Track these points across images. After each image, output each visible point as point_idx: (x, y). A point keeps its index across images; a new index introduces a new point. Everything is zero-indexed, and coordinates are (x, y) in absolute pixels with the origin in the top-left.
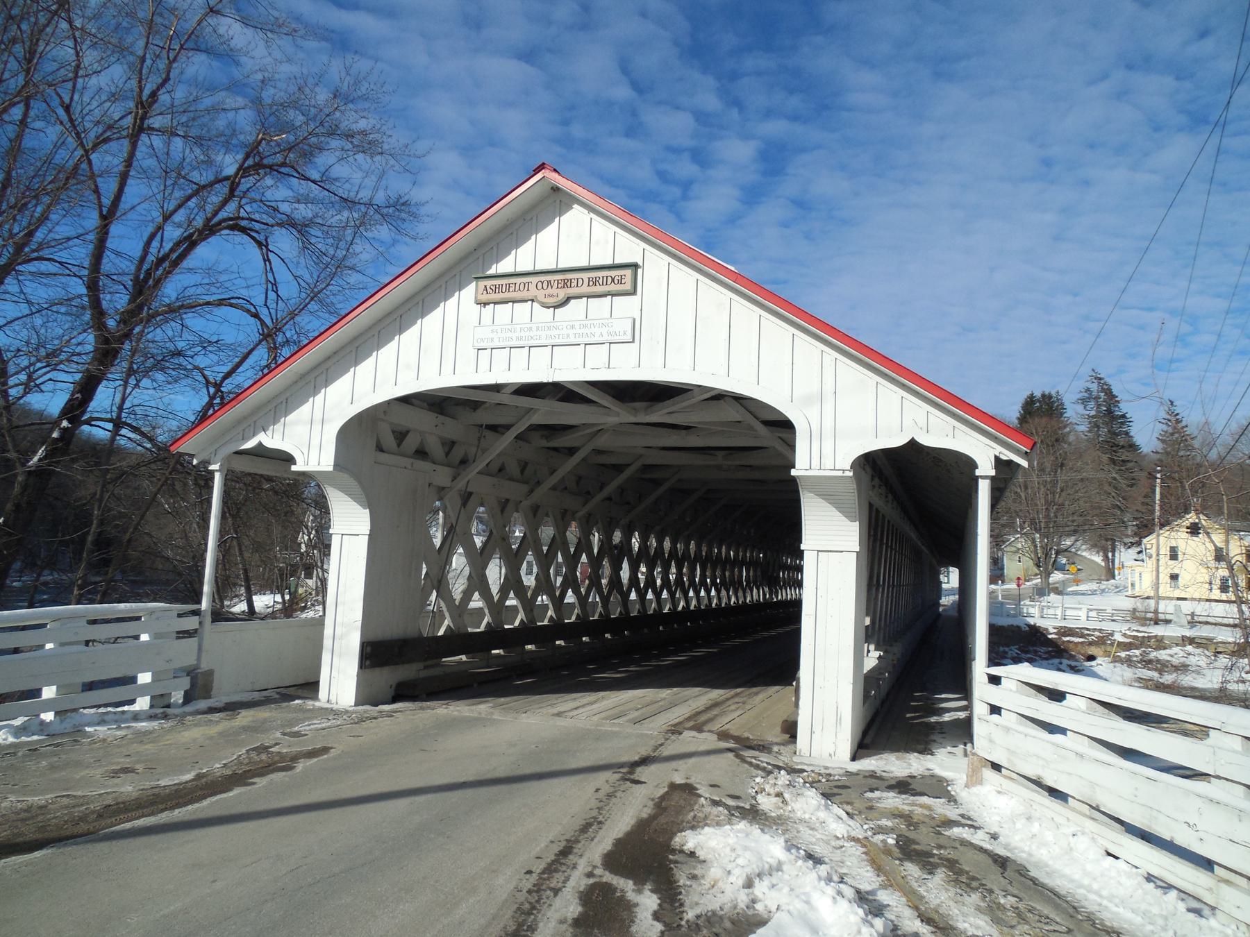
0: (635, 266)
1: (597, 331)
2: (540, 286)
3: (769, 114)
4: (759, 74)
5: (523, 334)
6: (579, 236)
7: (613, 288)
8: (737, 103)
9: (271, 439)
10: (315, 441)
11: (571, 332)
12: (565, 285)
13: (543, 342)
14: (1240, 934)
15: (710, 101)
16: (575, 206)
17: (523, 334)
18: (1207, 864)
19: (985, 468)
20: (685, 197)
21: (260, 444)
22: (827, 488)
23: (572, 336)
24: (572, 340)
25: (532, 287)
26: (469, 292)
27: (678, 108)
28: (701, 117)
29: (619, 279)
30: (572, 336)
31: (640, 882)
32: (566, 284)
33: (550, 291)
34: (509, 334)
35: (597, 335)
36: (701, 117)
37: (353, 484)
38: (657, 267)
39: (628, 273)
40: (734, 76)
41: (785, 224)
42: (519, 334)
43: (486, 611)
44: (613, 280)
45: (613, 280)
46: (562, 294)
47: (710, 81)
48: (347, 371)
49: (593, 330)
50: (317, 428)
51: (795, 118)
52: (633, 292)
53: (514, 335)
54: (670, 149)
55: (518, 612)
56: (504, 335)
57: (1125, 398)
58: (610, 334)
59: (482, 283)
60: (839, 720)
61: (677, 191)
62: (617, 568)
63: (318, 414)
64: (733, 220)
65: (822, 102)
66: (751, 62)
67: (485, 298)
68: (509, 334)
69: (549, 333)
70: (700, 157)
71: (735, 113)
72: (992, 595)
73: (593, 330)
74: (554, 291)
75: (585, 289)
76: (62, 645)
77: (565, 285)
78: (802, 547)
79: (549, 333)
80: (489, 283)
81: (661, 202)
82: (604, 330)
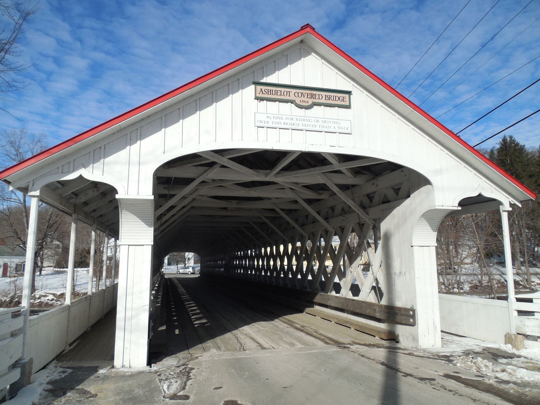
0: (349, 93)
2: (296, 94)
3: (95, 49)
4: (92, 29)
5: (288, 121)
6: (310, 70)
8: (80, 40)
9: (93, 173)
10: (134, 177)
11: (317, 124)
12: (312, 97)
13: (300, 127)
15: (66, 36)
16: (313, 54)
20: (48, 80)
21: (81, 177)
23: (318, 127)
24: (318, 129)
26: (250, 91)
27: (48, 35)
28: (60, 42)
29: (338, 99)
30: (318, 127)
32: (312, 96)
33: (302, 98)
34: (279, 121)
35: (332, 127)
36: (60, 42)
38: (360, 98)
39: (347, 96)
40: (80, 27)
41: (100, 102)
43: (356, 298)
44: (339, 99)
45: (339, 99)
46: (310, 101)
47: (66, 26)
48: (160, 130)
49: (329, 125)
50: (134, 169)
51: (108, 53)
52: (348, 107)
53: (282, 121)
54: (42, 54)
55: (336, 293)
59: (259, 87)
61: (43, 76)
63: (135, 158)
64: (73, 95)
65: (121, 50)
66: (88, 22)
67: (261, 95)
68: (279, 121)
69: (291, 121)
70: (57, 61)
71: (78, 44)
73: (329, 125)
74: (305, 99)
75: (323, 101)
77: (312, 97)
79: (291, 121)
80: (264, 88)
81: (35, 80)
82: (336, 126)
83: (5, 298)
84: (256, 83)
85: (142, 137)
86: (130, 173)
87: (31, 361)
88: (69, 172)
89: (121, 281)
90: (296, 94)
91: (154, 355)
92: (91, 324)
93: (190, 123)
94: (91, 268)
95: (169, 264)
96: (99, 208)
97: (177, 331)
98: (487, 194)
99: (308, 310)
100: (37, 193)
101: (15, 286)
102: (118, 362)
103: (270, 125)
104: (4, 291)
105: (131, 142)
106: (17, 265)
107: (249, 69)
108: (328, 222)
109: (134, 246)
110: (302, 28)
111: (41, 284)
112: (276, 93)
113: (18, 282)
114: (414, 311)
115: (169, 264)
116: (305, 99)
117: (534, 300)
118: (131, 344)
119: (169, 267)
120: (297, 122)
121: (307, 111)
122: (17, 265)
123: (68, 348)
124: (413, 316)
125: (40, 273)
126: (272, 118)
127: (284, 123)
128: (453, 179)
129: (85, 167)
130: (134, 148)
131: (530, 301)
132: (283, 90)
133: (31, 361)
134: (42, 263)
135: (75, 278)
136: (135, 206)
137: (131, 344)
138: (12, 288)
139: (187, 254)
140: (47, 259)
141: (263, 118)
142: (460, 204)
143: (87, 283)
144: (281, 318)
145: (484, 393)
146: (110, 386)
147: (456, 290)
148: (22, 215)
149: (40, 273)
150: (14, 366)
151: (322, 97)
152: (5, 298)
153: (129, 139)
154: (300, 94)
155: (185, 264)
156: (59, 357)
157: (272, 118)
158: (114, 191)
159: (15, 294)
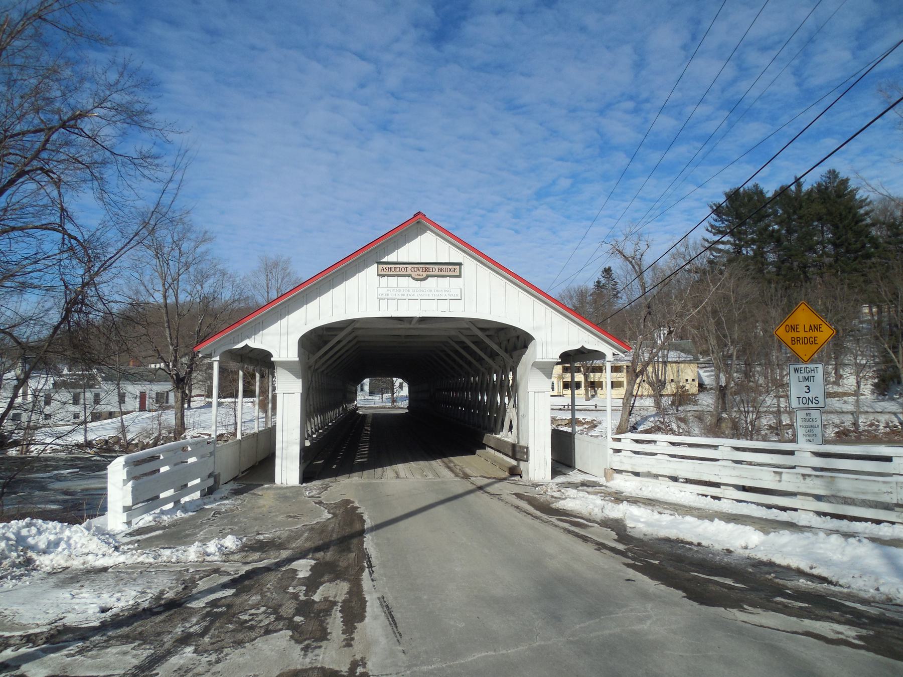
0: (460, 264)
1: (444, 294)
6: (426, 247)
7: (450, 273)
9: (254, 343)
10: (284, 344)
12: (425, 270)
13: (416, 297)
14: (901, 401)
18: (717, 485)
24: (431, 297)
29: (452, 270)
32: (427, 270)
39: (458, 267)
52: (459, 276)
59: (381, 266)
60: (546, 463)
63: (284, 331)
67: (383, 273)
72: (268, 404)
74: (421, 273)
75: (436, 273)
76: (175, 465)
77: (425, 270)
80: (384, 266)
83: (148, 440)
84: (379, 263)
85: (289, 313)
86: (281, 340)
87: (219, 474)
88: (238, 343)
89: (279, 419)
91: (306, 477)
92: (259, 460)
93: (325, 300)
94: (256, 400)
95: (371, 393)
96: (262, 362)
97: (334, 467)
98: (589, 347)
99: (478, 451)
100: (218, 358)
101: (160, 424)
102: (278, 480)
103: (390, 297)
104: (145, 430)
105: (281, 317)
106: (157, 393)
107: (371, 253)
108: (494, 360)
109: (289, 392)
110: (415, 216)
111: (192, 420)
112: (390, 269)
113: (162, 419)
114: (527, 448)
115: (371, 393)
116: (421, 273)
117: (894, 459)
118: (287, 470)
119: (370, 398)
122: (157, 393)
123: (241, 475)
124: (527, 453)
125: (189, 406)
128: (554, 334)
129: (249, 337)
130: (284, 321)
131: (791, 453)
132: (401, 266)
133: (219, 474)
134: (190, 391)
135: (897, 628)
136: (287, 365)
137: (287, 470)
138: (155, 426)
139: (395, 379)
140: (196, 385)
141: (384, 291)
142: (561, 357)
143: (252, 420)
144: (445, 460)
146: (271, 492)
148: (164, 327)
149: (189, 406)
150: (210, 476)
151: (435, 270)
152: (148, 440)
155: (393, 393)
156: (235, 479)
158: (269, 355)
159: (160, 435)
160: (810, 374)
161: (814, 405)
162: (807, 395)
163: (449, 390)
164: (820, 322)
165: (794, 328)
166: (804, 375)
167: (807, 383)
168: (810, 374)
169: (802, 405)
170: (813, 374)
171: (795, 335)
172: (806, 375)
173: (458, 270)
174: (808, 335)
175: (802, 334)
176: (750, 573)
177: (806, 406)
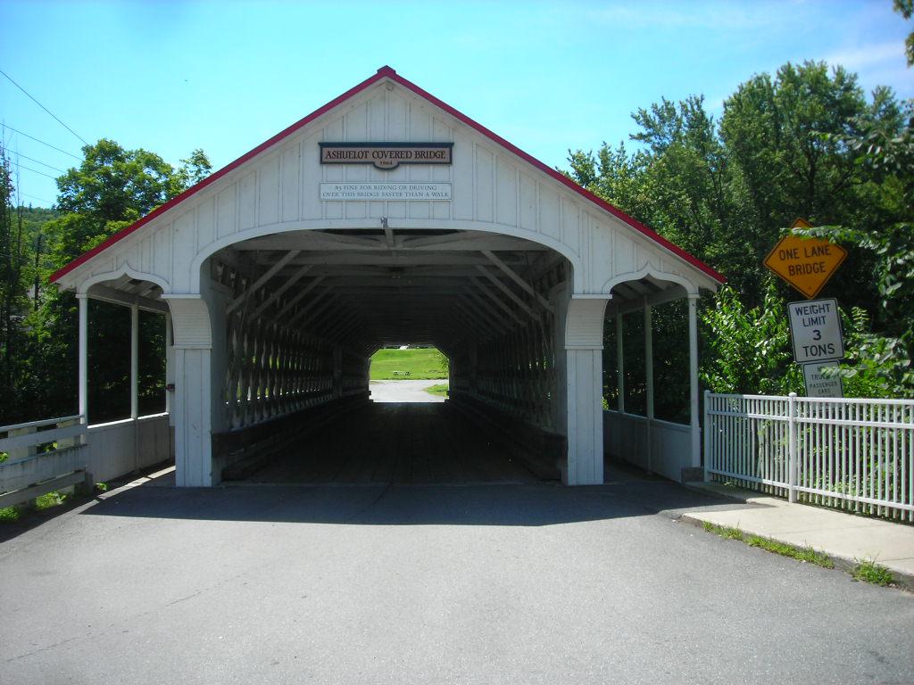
0: (450, 145)
2: (375, 155)
5: (364, 191)
7: (435, 160)
17: (364, 191)
19: (693, 296)
22: (587, 304)
25: (370, 155)
31: (903, 377)
33: (384, 159)
34: (352, 191)
37: (656, 284)
39: (447, 150)
42: (359, 191)
44: (435, 155)
46: (395, 162)
56: (346, 191)
57: (451, 171)
58: (434, 194)
62: (298, 367)
69: (385, 191)
73: (421, 191)
75: (413, 159)
78: (566, 347)
79: (385, 191)
82: (430, 192)
90: (375, 155)
120: (376, 191)
121: (390, 173)
126: (343, 188)
127: (358, 194)
145: (311, 249)
147: (703, 352)
153: (311, 286)
154: (380, 154)
157: (343, 188)
160: (819, 315)
161: (829, 356)
162: (817, 343)
163: (284, 372)
164: (790, 278)
165: (791, 254)
166: (810, 316)
167: (815, 327)
168: (819, 315)
169: (810, 357)
170: (823, 314)
171: (794, 262)
172: (814, 316)
173: (447, 155)
174: (811, 261)
175: (802, 261)
176: (882, 304)
177: (817, 357)
